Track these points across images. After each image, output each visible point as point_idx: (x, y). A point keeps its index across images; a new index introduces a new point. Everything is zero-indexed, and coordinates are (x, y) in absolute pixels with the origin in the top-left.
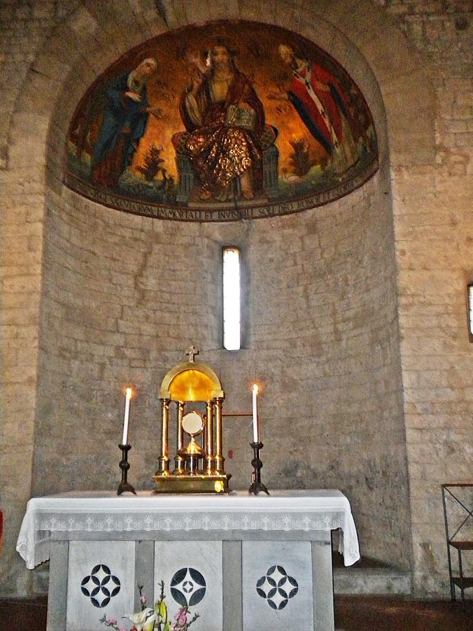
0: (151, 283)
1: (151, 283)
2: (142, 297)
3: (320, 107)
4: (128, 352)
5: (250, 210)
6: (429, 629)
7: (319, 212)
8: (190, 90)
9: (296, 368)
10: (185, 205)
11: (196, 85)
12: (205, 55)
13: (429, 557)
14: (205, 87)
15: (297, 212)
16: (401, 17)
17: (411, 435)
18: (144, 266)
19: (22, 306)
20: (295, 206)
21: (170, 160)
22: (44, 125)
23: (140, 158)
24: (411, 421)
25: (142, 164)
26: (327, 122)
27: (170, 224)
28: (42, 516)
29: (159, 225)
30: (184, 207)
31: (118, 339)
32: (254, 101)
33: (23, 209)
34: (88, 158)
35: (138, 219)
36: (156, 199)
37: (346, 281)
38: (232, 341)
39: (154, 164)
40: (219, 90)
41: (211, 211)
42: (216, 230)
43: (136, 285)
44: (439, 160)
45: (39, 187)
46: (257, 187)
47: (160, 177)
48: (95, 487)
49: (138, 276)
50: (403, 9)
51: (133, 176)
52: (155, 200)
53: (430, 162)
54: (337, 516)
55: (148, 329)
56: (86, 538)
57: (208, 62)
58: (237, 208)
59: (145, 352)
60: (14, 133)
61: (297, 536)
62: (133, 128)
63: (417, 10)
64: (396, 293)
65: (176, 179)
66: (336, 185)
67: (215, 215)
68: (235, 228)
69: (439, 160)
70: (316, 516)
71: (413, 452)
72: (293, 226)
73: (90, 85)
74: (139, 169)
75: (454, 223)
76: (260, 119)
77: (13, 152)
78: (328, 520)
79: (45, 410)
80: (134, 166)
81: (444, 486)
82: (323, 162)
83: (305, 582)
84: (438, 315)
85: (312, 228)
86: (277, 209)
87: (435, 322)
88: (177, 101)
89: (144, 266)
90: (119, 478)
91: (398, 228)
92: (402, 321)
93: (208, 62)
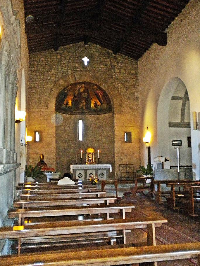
0: (67, 128)
1: (67, 128)
2: (65, 131)
3: (101, 97)
4: (64, 141)
6: (199, 31)
7: (99, 116)
13: (117, 175)
14: (79, 90)
16: (117, 87)
17: (115, 157)
19: (52, 134)
21: (70, 102)
22: (54, 101)
24: (116, 155)
25: (65, 104)
26: (102, 99)
27: (69, 115)
30: (72, 112)
31: (62, 139)
32: (88, 93)
37: (104, 130)
38: (81, 138)
39: (67, 103)
40: (82, 90)
42: (78, 117)
47: (68, 106)
50: (117, 86)
51: (63, 106)
52: (67, 110)
53: (120, 113)
54: (109, 167)
55: (67, 137)
56: (79, 170)
58: (82, 113)
59: (66, 141)
64: (114, 135)
66: (102, 111)
68: (82, 117)
71: (116, 160)
72: (93, 117)
76: (88, 96)
77: (49, 106)
81: (120, 165)
83: (105, 175)
85: (98, 118)
86: (90, 114)
91: (115, 124)
92: (115, 139)
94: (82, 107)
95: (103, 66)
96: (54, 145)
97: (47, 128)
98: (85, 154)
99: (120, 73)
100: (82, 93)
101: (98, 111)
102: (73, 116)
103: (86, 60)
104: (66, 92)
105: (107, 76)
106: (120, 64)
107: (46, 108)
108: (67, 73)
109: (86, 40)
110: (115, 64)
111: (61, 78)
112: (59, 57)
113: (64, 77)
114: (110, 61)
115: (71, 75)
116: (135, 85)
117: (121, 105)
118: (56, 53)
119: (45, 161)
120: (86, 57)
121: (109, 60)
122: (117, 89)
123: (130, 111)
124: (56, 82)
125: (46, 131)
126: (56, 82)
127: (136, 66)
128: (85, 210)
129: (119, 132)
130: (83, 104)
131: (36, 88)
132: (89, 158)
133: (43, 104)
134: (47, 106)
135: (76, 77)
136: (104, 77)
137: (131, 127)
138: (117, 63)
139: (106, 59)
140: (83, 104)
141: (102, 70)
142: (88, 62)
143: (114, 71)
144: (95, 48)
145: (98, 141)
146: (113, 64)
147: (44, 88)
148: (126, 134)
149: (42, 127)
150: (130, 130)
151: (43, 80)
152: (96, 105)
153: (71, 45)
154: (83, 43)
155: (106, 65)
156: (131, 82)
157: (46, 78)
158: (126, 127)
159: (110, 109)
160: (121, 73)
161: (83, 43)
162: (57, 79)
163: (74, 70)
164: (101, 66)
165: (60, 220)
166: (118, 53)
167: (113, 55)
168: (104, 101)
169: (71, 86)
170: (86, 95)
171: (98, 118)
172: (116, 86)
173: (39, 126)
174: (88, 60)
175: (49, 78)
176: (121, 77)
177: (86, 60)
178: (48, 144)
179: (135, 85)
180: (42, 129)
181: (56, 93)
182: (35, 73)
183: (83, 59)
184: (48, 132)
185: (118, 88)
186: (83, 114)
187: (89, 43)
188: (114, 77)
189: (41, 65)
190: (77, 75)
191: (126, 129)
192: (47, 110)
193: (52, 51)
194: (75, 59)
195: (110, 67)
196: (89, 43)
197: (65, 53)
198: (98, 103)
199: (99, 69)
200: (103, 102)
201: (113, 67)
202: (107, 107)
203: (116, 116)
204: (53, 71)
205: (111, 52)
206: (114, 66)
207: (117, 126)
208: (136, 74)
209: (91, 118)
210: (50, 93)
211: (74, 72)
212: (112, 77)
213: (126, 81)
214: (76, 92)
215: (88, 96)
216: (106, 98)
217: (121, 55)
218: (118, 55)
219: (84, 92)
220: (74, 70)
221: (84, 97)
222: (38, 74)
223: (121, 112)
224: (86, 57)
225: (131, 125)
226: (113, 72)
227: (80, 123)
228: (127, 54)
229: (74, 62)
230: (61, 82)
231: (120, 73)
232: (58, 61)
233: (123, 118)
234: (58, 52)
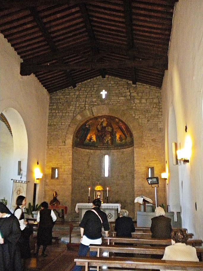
1: (90, 163)
5: (134, 32)
8: (98, 125)
9: (119, 181)
10: (97, 146)
11: (100, 124)
12: (102, 119)
14: (102, 124)
15: (120, 149)
18: (89, 160)
20: (120, 148)
21: (94, 138)
22: (72, 137)
23: (88, 138)
25: (89, 139)
28: (78, 206)
29: (92, 151)
33: (68, 153)
34: (78, 140)
35: (88, 150)
36: (91, 146)
38: (106, 175)
39: (91, 139)
40: (104, 124)
41: (103, 148)
42: (103, 152)
43: (87, 164)
44: (143, 146)
45: (71, 149)
46: (112, 143)
47: (92, 141)
48: (86, 202)
49: (88, 162)
50: (138, 117)
52: (91, 146)
53: (141, 147)
57: (102, 120)
60: (66, 139)
61: (112, 209)
62: (87, 132)
63: (140, 117)
65: (95, 141)
66: (127, 145)
67: (103, 149)
68: (108, 151)
69: (143, 146)
70: (115, 207)
72: (120, 152)
73: (49, 17)
74: (88, 140)
75: (145, 158)
76: (113, 130)
77: (66, 142)
78: (116, 207)
79: (73, 189)
80: (87, 139)
82: (125, 139)
83: (114, 215)
84: (141, 175)
87: (140, 176)
88: (96, 126)
89: (89, 160)
90: (88, 201)
91: (135, 159)
93: (102, 120)
94: (108, 141)
95: (122, 98)
96: (70, 182)
97: (65, 165)
98: (93, 191)
99: (140, 103)
100: (105, 127)
101: (123, 146)
102: (98, 152)
103: (104, 93)
104: (87, 127)
105: (125, 108)
106: (140, 94)
107: (64, 144)
108: (84, 108)
109: (103, 73)
110: (134, 94)
111: (79, 113)
112: (77, 93)
113: (81, 113)
114: (130, 92)
115: (89, 109)
116: (157, 115)
117: (142, 137)
118: (75, 90)
119: (58, 198)
120: (104, 91)
121: (128, 91)
122: (138, 120)
123: (153, 143)
124: (74, 118)
125: (63, 167)
126: (74, 118)
127: (159, 94)
128: (118, 249)
129: (140, 167)
130: (108, 138)
131: (55, 125)
132: (98, 196)
133: (61, 141)
134: (65, 143)
135: (93, 111)
136: (123, 108)
137: (154, 162)
138: (138, 94)
139: (125, 90)
140: (108, 138)
141: (120, 102)
142: (106, 95)
143: (134, 102)
144: (111, 80)
145: (123, 177)
146: (133, 94)
147: (62, 124)
148: (150, 169)
149: (59, 164)
150: (152, 165)
151: (61, 117)
152: (120, 138)
153: (89, 80)
154: (101, 77)
155: (125, 96)
156: (154, 111)
157: (64, 114)
158: (148, 161)
159: (132, 144)
160: (142, 103)
161: (101, 77)
162: (75, 115)
163: (92, 105)
164: (120, 98)
165: (120, 255)
166: (137, 83)
167: (133, 85)
168: (128, 135)
169: (91, 121)
170: (110, 129)
171: (123, 153)
172: (136, 117)
173: (57, 162)
174: (106, 93)
175: (67, 114)
176: (142, 108)
177: (104, 93)
178: (64, 182)
179: (157, 115)
180: (59, 166)
181: (73, 129)
182: (54, 111)
183: (101, 93)
184: (65, 168)
185: (139, 119)
186: (108, 148)
187: (107, 76)
188: (133, 108)
189: (60, 103)
190: (95, 109)
191: (148, 163)
192: (65, 147)
193: (71, 88)
194: (93, 93)
195: (129, 98)
196: (107, 76)
197: (83, 89)
198: (123, 136)
199: (118, 102)
200: (127, 136)
201: (132, 98)
202: (128, 142)
203: (136, 150)
204: (71, 107)
205: (131, 82)
206: (134, 96)
207: (138, 160)
208: (159, 102)
209: (115, 152)
210: (68, 130)
211: (91, 106)
212: (132, 109)
213: (147, 111)
214: (99, 126)
215: (113, 130)
216: (127, 132)
217: (142, 85)
218: (139, 85)
219: (107, 125)
220: (92, 105)
221: (109, 131)
222: (57, 112)
223: (141, 145)
224: (104, 91)
225: (154, 159)
226: (133, 103)
227: (107, 158)
228: (147, 83)
229: (92, 97)
230: (79, 117)
231: (140, 103)
232: (77, 97)
233: (144, 151)
234: (76, 88)
